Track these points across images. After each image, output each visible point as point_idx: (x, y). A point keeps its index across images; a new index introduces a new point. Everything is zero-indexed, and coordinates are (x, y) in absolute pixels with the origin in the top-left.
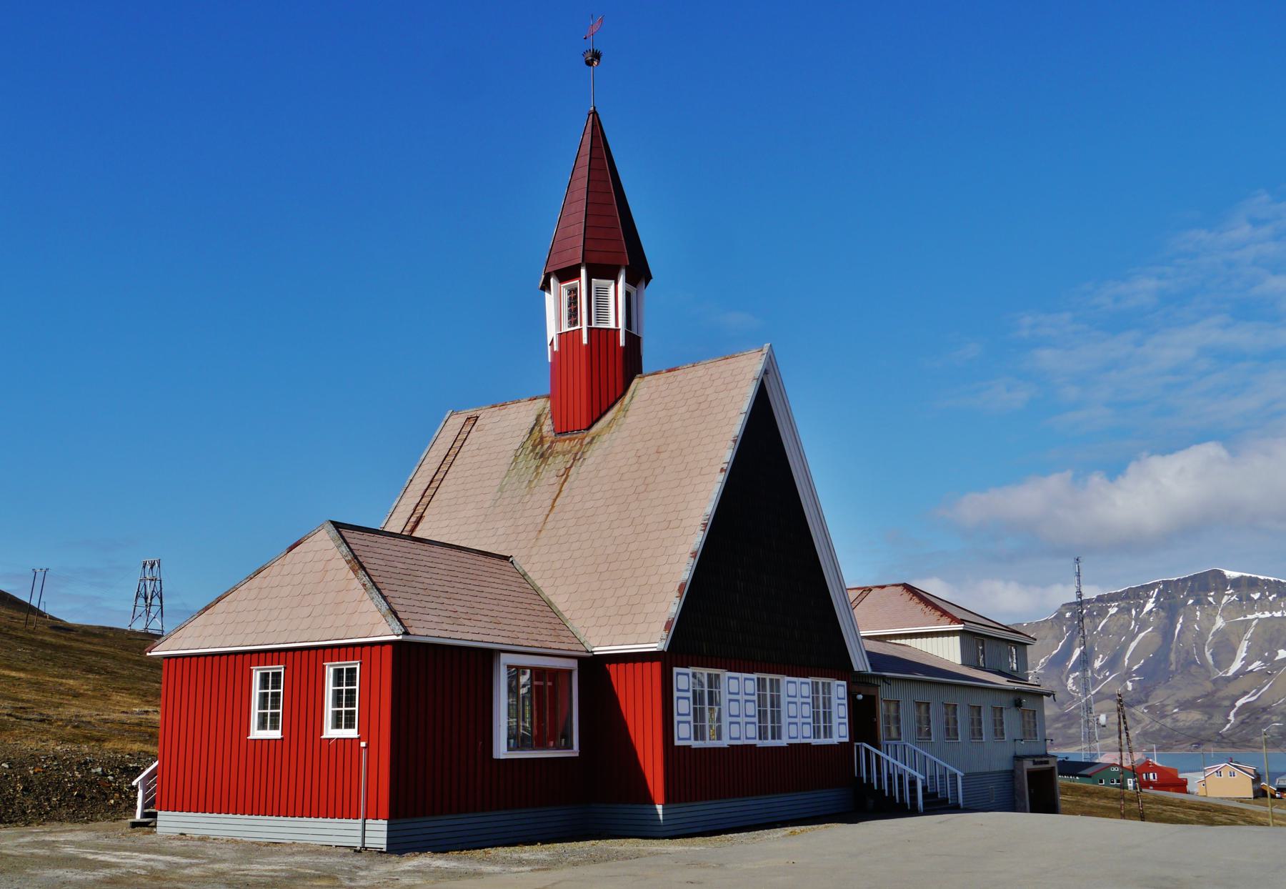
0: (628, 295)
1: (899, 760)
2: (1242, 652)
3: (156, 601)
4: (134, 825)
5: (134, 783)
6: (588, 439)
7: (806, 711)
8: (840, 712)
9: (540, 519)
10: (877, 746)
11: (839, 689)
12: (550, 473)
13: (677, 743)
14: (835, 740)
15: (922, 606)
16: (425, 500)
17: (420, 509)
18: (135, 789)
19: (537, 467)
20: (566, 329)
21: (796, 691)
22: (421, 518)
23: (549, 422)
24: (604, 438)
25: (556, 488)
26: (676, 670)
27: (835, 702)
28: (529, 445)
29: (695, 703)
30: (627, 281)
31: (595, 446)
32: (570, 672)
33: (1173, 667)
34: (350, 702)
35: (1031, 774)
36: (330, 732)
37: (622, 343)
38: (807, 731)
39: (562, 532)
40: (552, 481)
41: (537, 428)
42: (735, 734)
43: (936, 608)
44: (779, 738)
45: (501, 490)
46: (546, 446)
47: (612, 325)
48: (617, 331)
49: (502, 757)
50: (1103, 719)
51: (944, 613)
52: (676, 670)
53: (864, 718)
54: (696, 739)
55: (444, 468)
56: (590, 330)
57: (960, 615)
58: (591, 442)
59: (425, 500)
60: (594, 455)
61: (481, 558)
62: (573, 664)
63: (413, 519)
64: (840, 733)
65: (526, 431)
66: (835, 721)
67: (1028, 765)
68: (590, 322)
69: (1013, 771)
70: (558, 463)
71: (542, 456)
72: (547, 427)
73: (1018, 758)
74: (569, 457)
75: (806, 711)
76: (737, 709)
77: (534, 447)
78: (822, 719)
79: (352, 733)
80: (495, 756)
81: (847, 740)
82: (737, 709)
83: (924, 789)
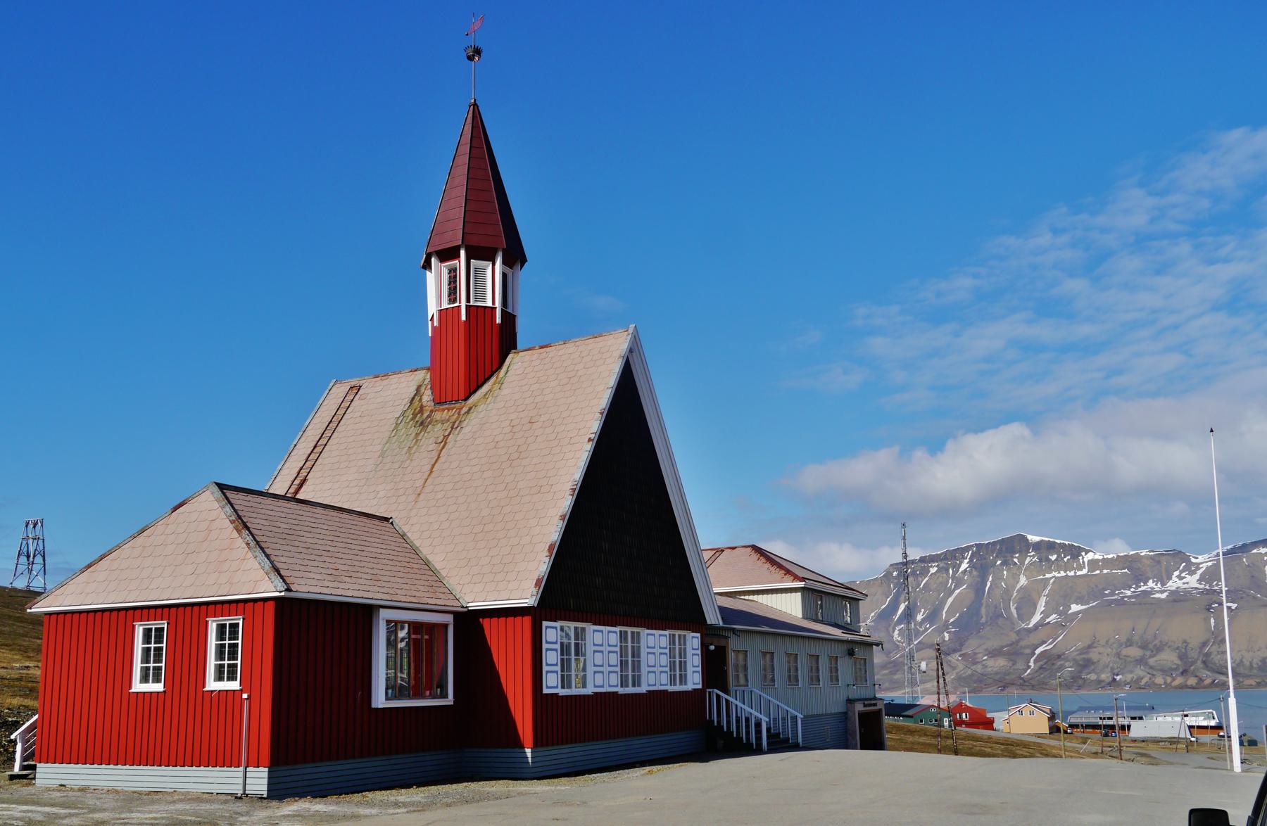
0: (504, 276)
1: (747, 704)
2: (1041, 607)
3: (39, 559)
4: (13, 777)
5: (13, 737)
6: (465, 409)
7: (662, 661)
8: (694, 662)
9: (419, 483)
10: (726, 691)
11: (693, 641)
12: (429, 440)
13: (545, 691)
14: (689, 687)
15: (768, 565)
16: (309, 464)
17: (304, 473)
18: (14, 742)
19: (417, 434)
20: (445, 306)
21: (654, 641)
22: (304, 480)
23: (429, 392)
24: (481, 408)
25: (435, 454)
26: (545, 624)
27: (689, 652)
28: (410, 413)
29: (562, 654)
30: (504, 262)
31: (472, 415)
32: (446, 626)
33: (983, 620)
34: (233, 655)
35: (862, 715)
36: (212, 685)
37: (498, 320)
38: (665, 679)
39: (440, 495)
40: (431, 447)
41: (417, 398)
42: (599, 682)
43: (781, 567)
44: (639, 685)
45: (382, 455)
46: (425, 415)
47: (489, 304)
49: (380, 706)
50: (923, 665)
51: (788, 572)
52: (545, 624)
53: (715, 667)
54: (563, 687)
55: (328, 434)
56: (467, 307)
57: (801, 574)
58: (468, 412)
59: (309, 464)
60: (471, 424)
61: (362, 519)
62: (449, 619)
63: (297, 482)
64: (694, 680)
65: (407, 401)
66: (690, 669)
67: (859, 707)
68: (468, 300)
69: (846, 713)
70: (437, 431)
71: (422, 424)
72: (427, 397)
73: (850, 701)
74: (447, 426)
75: (662, 661)
76: (602, 659)
77: (415, 415)
78: (677, 668)
79: (235, 685)
80: (373, 706)
81: (700, 686)
82: (602, 659)
83: (768, 730)
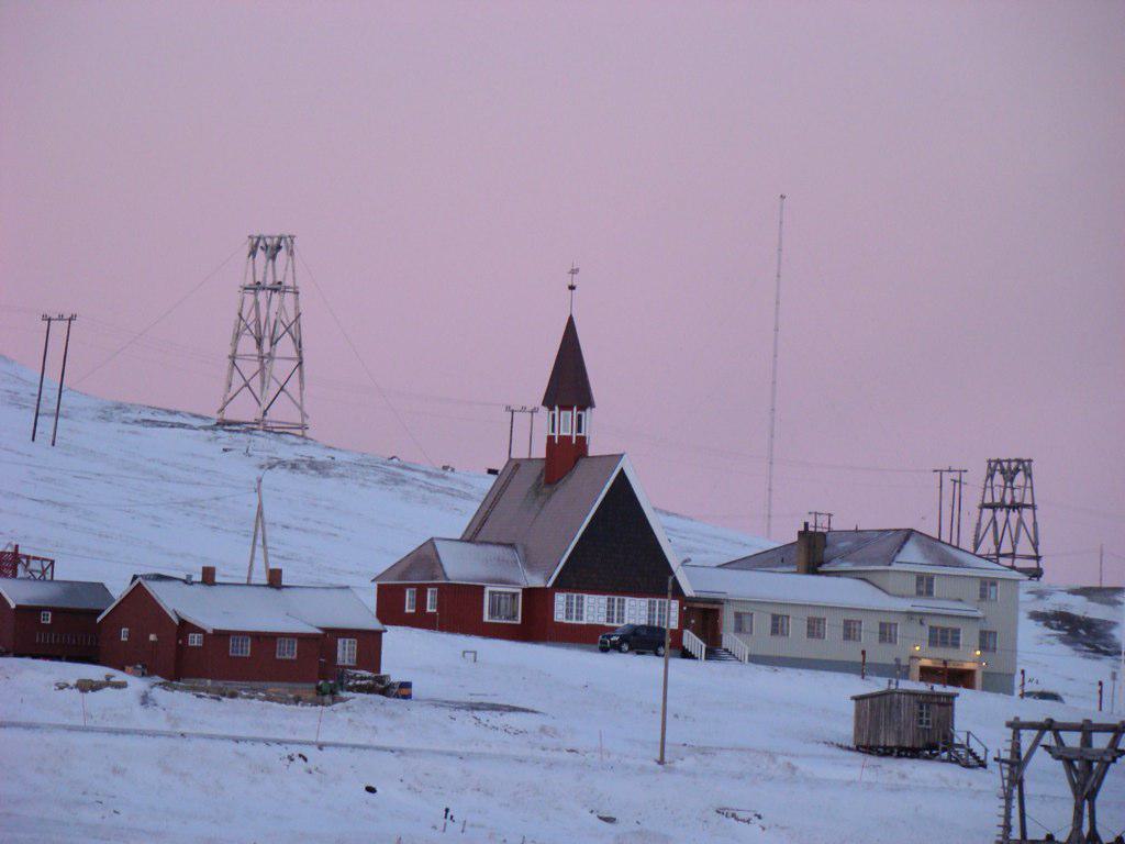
3: (286, 346)
47: (569, 434)
48: (571, 438)
